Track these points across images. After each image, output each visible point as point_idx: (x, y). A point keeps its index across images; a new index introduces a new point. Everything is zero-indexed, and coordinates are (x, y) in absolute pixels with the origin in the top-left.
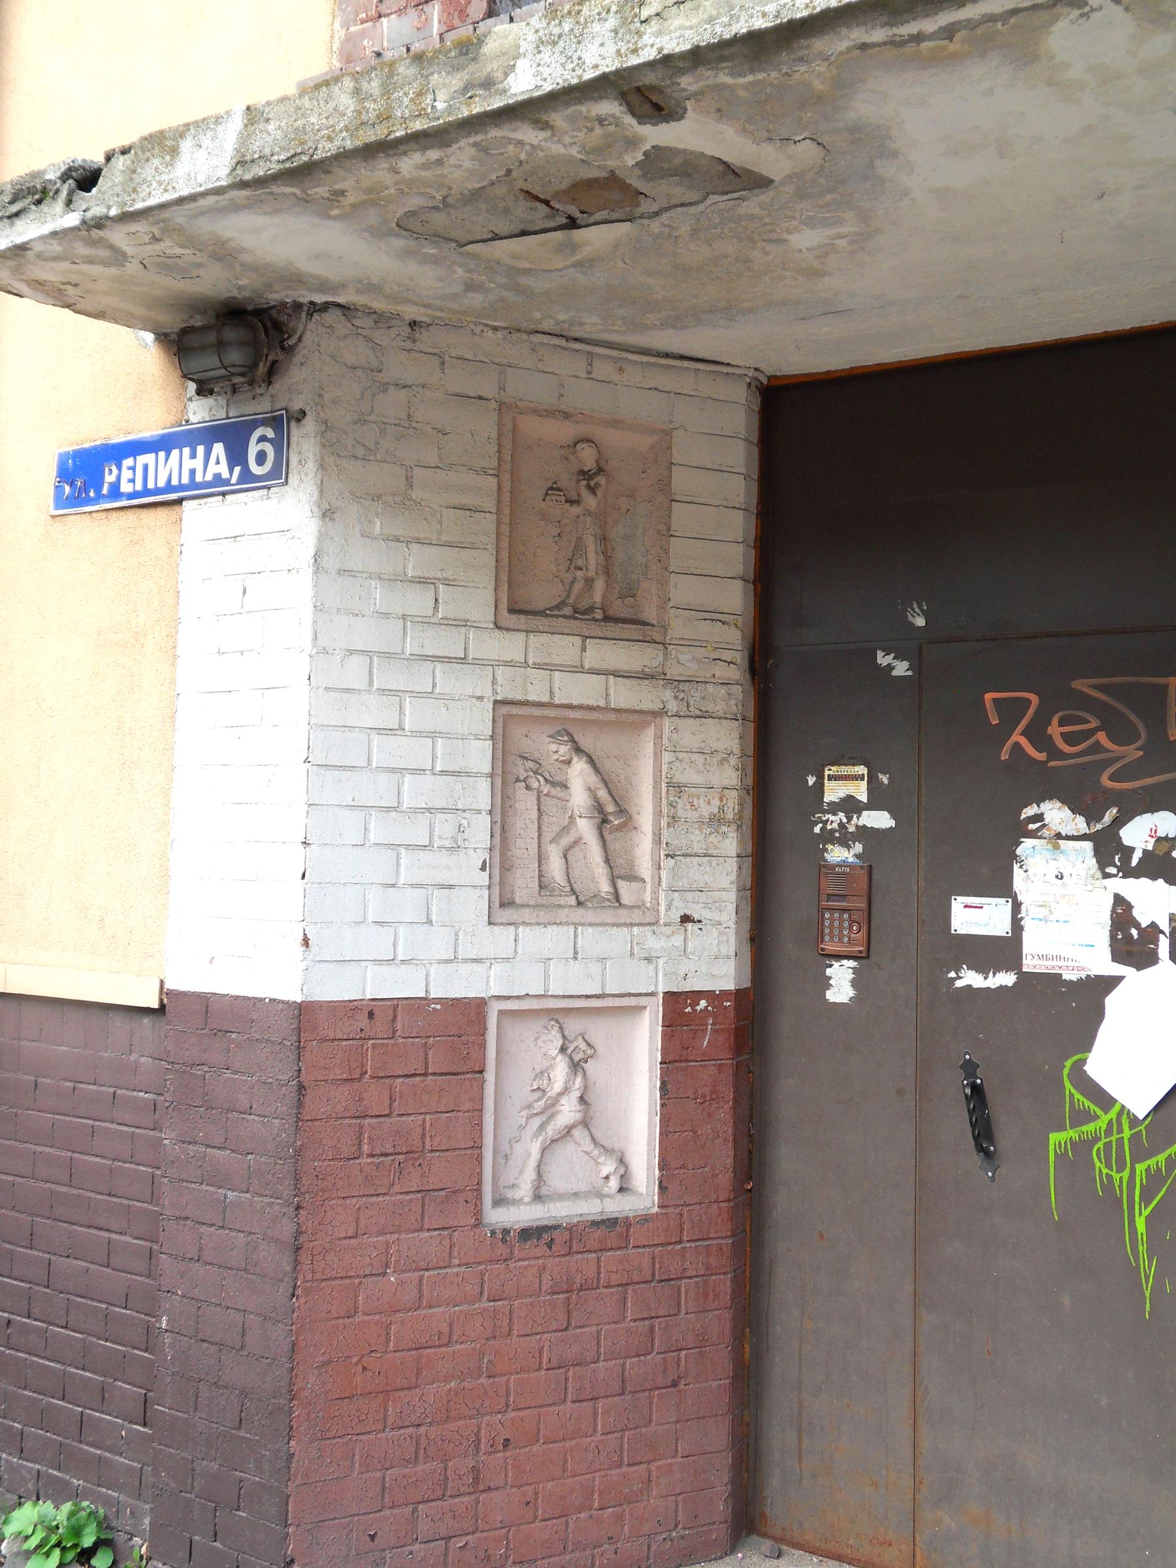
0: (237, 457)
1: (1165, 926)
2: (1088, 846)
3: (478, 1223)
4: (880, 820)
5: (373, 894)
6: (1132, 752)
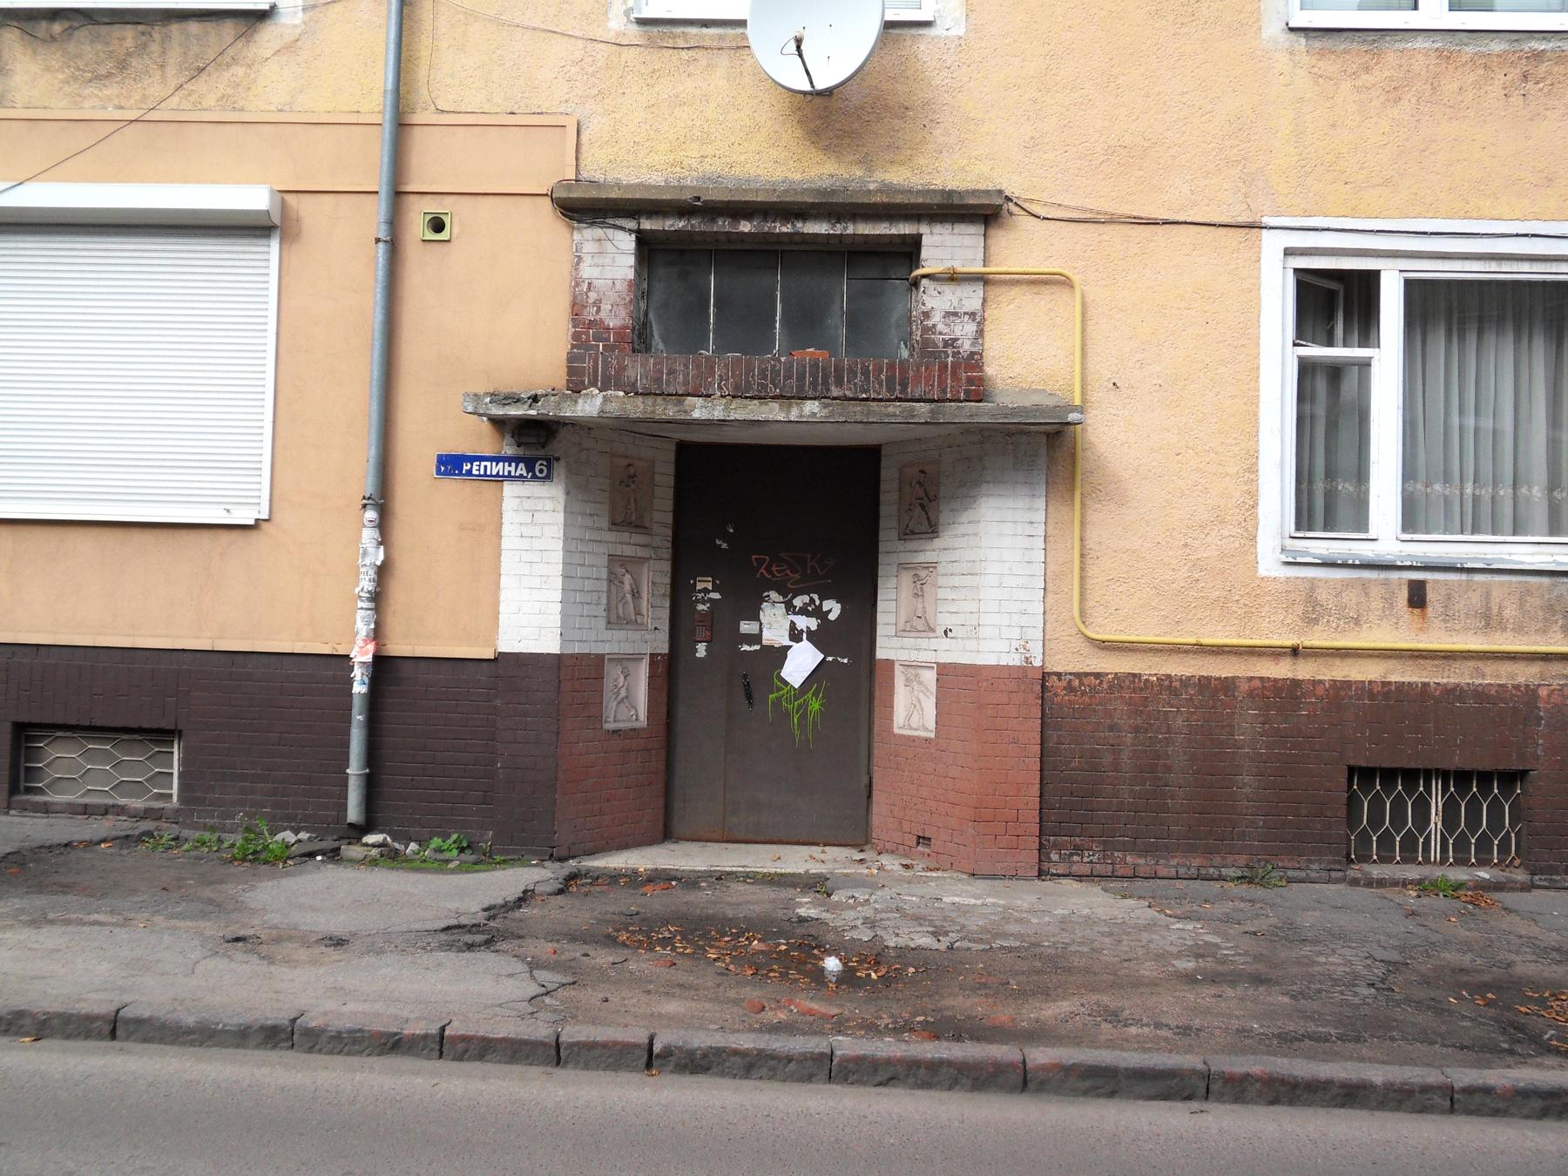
0: (530, 468)
1: (805, 630)
2: (783, 605)
3: (601, 728)
4: (716, 596)
5: (577, 619)
6: (797, 576)
